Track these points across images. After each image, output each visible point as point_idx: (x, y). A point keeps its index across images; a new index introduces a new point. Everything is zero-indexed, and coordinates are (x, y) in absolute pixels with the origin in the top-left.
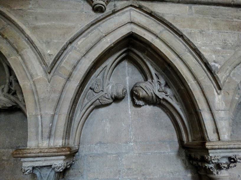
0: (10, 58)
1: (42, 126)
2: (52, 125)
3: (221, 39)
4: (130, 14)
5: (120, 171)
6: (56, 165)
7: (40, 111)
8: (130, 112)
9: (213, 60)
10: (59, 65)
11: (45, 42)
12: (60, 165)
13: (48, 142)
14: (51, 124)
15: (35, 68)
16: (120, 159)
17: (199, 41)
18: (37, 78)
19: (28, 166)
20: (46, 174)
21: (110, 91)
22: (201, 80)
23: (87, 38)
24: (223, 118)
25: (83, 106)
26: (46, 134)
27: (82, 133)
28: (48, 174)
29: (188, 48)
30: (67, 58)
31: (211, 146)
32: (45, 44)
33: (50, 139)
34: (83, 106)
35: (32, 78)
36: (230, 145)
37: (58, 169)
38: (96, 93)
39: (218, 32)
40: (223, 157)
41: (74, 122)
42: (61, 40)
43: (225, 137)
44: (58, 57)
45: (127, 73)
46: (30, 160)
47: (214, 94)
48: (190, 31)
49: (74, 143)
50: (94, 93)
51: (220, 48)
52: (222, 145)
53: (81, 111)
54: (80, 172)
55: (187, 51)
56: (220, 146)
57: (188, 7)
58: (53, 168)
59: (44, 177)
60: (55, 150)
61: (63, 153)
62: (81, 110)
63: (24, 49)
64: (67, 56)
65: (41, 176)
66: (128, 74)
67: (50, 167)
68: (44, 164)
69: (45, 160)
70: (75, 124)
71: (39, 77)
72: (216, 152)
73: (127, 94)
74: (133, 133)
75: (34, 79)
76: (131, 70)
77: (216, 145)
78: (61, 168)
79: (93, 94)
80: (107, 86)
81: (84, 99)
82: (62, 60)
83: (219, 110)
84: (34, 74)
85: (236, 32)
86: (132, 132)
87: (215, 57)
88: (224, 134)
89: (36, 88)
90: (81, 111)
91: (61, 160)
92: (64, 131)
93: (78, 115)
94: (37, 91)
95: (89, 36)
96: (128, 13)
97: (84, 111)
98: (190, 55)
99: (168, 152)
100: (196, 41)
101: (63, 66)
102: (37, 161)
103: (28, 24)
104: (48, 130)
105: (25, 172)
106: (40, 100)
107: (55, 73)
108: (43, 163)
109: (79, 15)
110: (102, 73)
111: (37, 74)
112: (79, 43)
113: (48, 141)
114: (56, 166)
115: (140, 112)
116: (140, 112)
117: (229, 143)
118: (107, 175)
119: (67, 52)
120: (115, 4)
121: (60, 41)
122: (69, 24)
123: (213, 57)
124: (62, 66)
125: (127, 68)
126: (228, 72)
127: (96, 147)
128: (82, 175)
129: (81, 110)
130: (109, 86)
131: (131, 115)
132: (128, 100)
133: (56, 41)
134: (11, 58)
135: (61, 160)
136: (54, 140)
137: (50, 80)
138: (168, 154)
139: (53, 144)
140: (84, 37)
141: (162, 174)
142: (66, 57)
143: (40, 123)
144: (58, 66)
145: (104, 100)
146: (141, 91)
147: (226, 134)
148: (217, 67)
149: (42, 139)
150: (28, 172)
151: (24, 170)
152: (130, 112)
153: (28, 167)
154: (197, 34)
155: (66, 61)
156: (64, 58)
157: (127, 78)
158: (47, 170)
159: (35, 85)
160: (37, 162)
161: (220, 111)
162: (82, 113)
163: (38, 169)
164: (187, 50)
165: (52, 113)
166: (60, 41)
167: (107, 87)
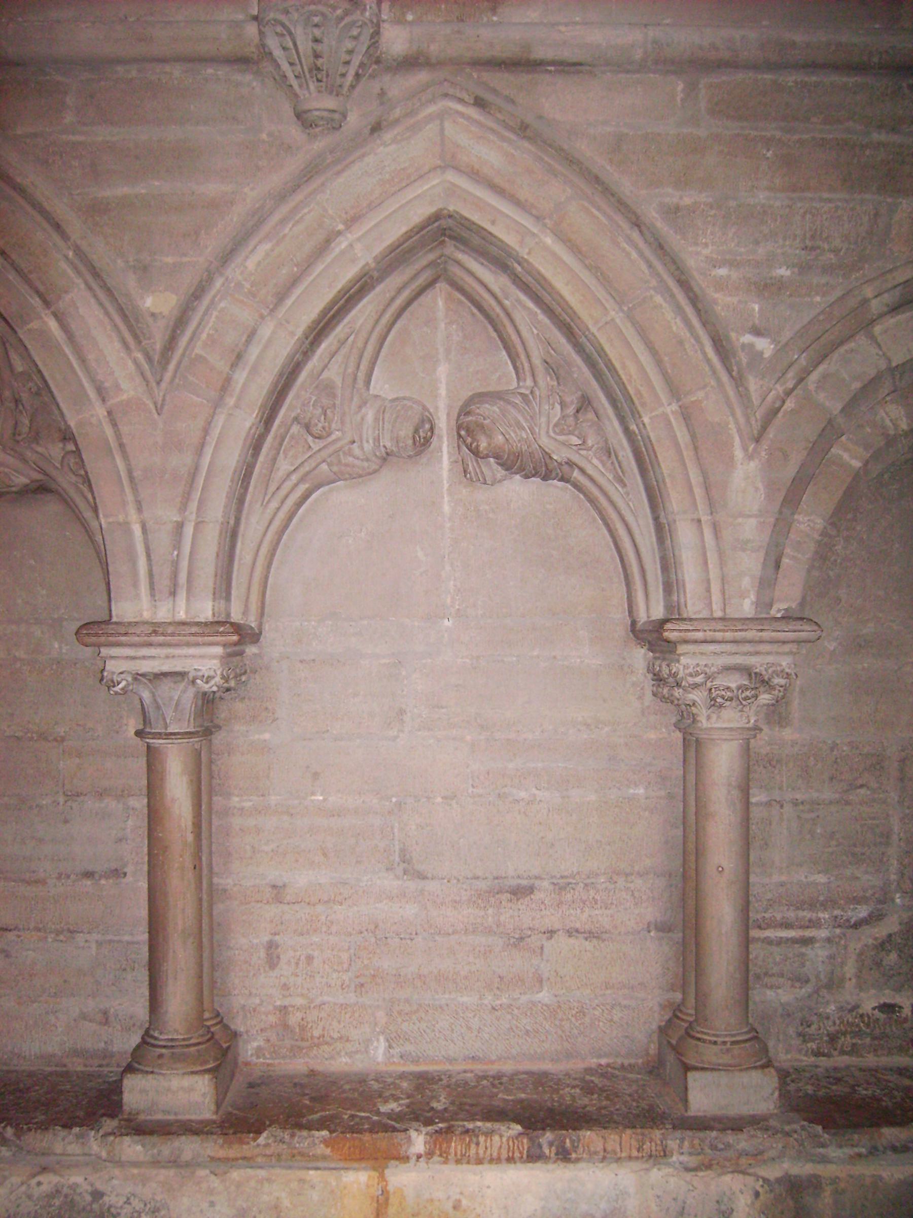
0: (26, 329)
1: (148, 556)
2: (178, 555)
3: (798, 232)
4: (442, 130)
5: (402, 712)
6: (199, 670)
7: (140, 510)
8: (447, 509)
9: (750, 324)
10: (185, 350)
11: (132, 263)
12: (212, 673)
13: (170, 606)
14: (176, 553)
15: (108, 363)
16: (404, 673)
17: (706, 245)
18: (119, 400)
19: (121, 670)
20: (171, 698)
21: (370, 432)
22: (692, 402)
23: (278, 244)
24: (748, 541)
25: (272, 489)
26: (163, 583)
27: (270, 581)
28: (176, 698)
29: (658, 275)
30: (210, 325)
31: (680, 631)
32: (135, 273)
33: (177, 599)
34: (272, 489)
35: (104, 400)
36: (746, 630)
37: (207, 682)
38: (316, 438)
39: (791, 199)
40: (728, 669)
41: (243, 544)
42: (185, 255)
43: (742, 605)
44: (181, 321)
45: (441, 350)
46: (125, 655)
47: (732, 457)
48: (675, 200)
49: (245, 612)
50: (310, 439)
51: (788, 273)
52: (719, 631)
53: (266, 506)
54: (267, 709)
55: (654, 288)
56: (711, 633)
57: (681, 86)
58: (191, 679)
59: (164, 704)
60: (194, 630)
61: (219, 639)
62: (267, 499)
63: (66, 292)
64: (213, 319)
65: (155, 701)
66: (448, 351)
67: (179, 678)
68: (165, 668)
69: (167, 657)
70: (244, 551)
71: (125, 397)
72: (702, 654)
73: (440, 438)
74: (455, 586)
75: (111, 402)
76: (461, 334)
77: (699, 630)
78: (213, 682)
79: (306, 440)
80: (357, 413)
81: (274, 460)
82: (194, 334)
83: (741, 515)
84: (107, 385)
85: (868, 196)
86: (452, 583)
87: (761, 309)
88: (743, 595)
89: (118, 435)
90: (265, 506)
91: (214, 657)
92: (216, 576)
93: (254, 520)
94: (122, 446)
95: (285, 236)
96: (431, 129)
97: (274, 505)
98: (664, 305)
99: (580, 657)
100: (696, 244)
101: (201, 356)
102: (144, 658)
103: (71, 194)
104: (167, 571)
105: (114, 686)
106: (135, 474)
107: (177, 380)
108: (163, 664)
109: (247, 147)
110: (339, 358)
111: (118, 388)
112: (251, 264)
113: (171, 602)
114: (200, 674)
115: (487, 507)
116: (487, 507)
117: (743, 624)
118: (360, 723)
119: (212, 302)
120: (382, 89)
121: (185, 259)
122: (212, 188)
123: (754, 310)
124: (197, 355)
125: (443, 325)
126: (790, 374)
127: (320, 630)
128: (274, 720)
129: (267, 499)
130: (364, 410)
131: (450, 519)
132: (440, 461)
133: (169, 260)
134: (30, 326)
135: (214, 657)
136: (188, 599)
137: (163, 405)
138: (582, 662)
139: (187, 612)
140: (267, 237)
141: (551, 727)
142: (208, 322)
143: (140, 548)
144: (183, 355)
145: (347, 465)
146: (485, 433)
147: (749, 597)
148: (761, 353)
149: (153, 595)
150: (121, 686)
151: (113, 681)
152: (447, 509)
153: (121, 673)
154: (703, 210)
155: (208, 335)
156: (203, 323)
157: (442, 371)
158: (172, 685)
159: (115, 425)
160: (145, 662)
161: (740, 520)
162: (268, 511)
163: (146, 681)
164: (654, 283)
165: (175, 519)
166: (185, 259)
167: (359, 417)
